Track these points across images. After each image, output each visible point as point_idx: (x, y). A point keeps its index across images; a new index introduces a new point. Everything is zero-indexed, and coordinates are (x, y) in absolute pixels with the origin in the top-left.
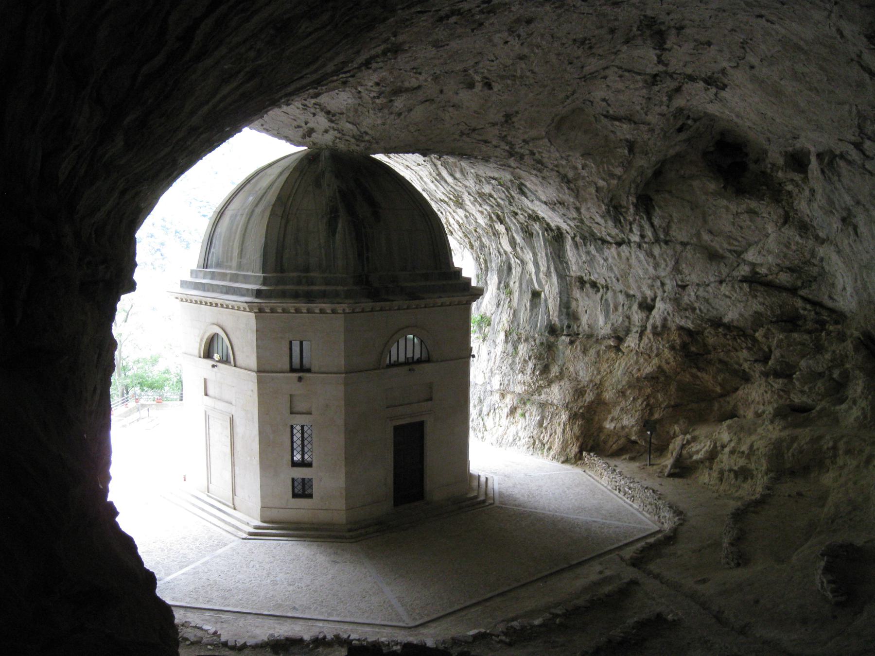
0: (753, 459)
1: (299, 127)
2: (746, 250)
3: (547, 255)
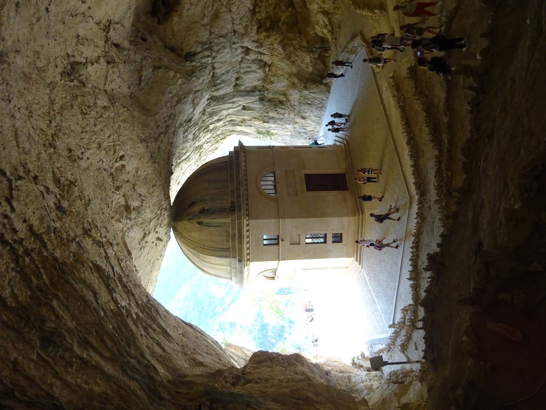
1: (156, 245)
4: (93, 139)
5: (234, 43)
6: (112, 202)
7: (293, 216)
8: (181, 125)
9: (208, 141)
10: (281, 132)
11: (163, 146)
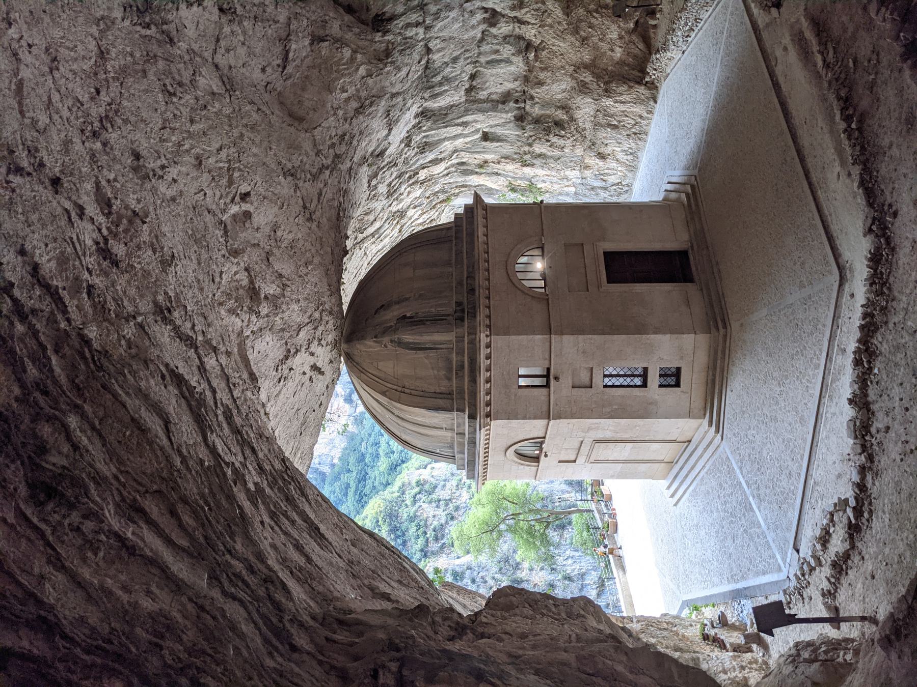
1: (311, 379)
4: (187, 147)
6: (221, 273)
7: (578, 330)
10: (556, 187)
11: (328, 193)
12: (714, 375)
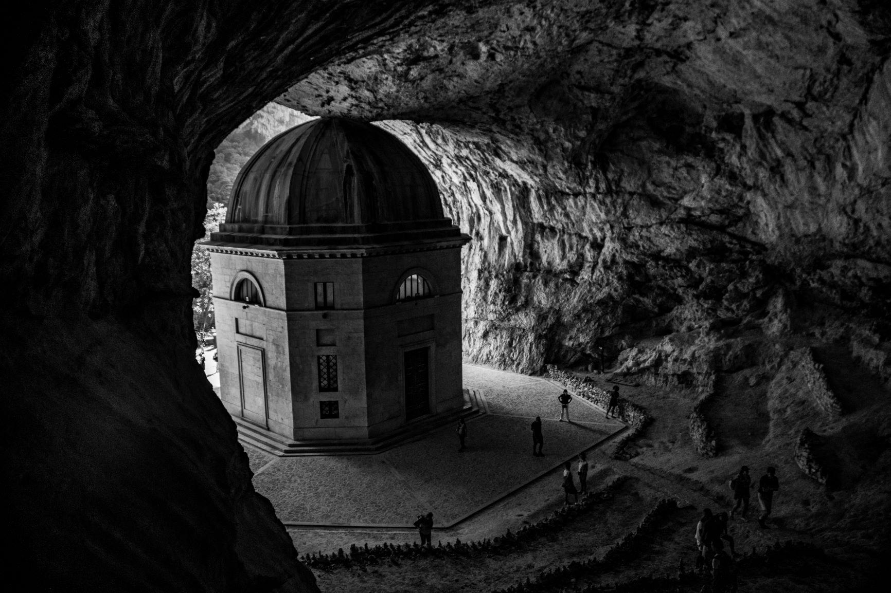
0: (695, 365)
2: (682, 198)
3: (513, 206)
4: (544, 22)
5: (612, 227)
7: (368, 331)
8: (495, 140)
9: (447, 178)
12: (335, 445)
